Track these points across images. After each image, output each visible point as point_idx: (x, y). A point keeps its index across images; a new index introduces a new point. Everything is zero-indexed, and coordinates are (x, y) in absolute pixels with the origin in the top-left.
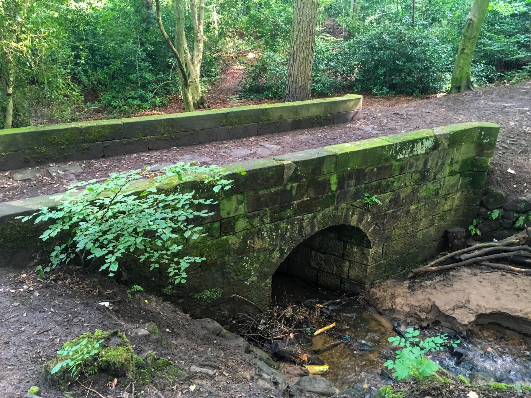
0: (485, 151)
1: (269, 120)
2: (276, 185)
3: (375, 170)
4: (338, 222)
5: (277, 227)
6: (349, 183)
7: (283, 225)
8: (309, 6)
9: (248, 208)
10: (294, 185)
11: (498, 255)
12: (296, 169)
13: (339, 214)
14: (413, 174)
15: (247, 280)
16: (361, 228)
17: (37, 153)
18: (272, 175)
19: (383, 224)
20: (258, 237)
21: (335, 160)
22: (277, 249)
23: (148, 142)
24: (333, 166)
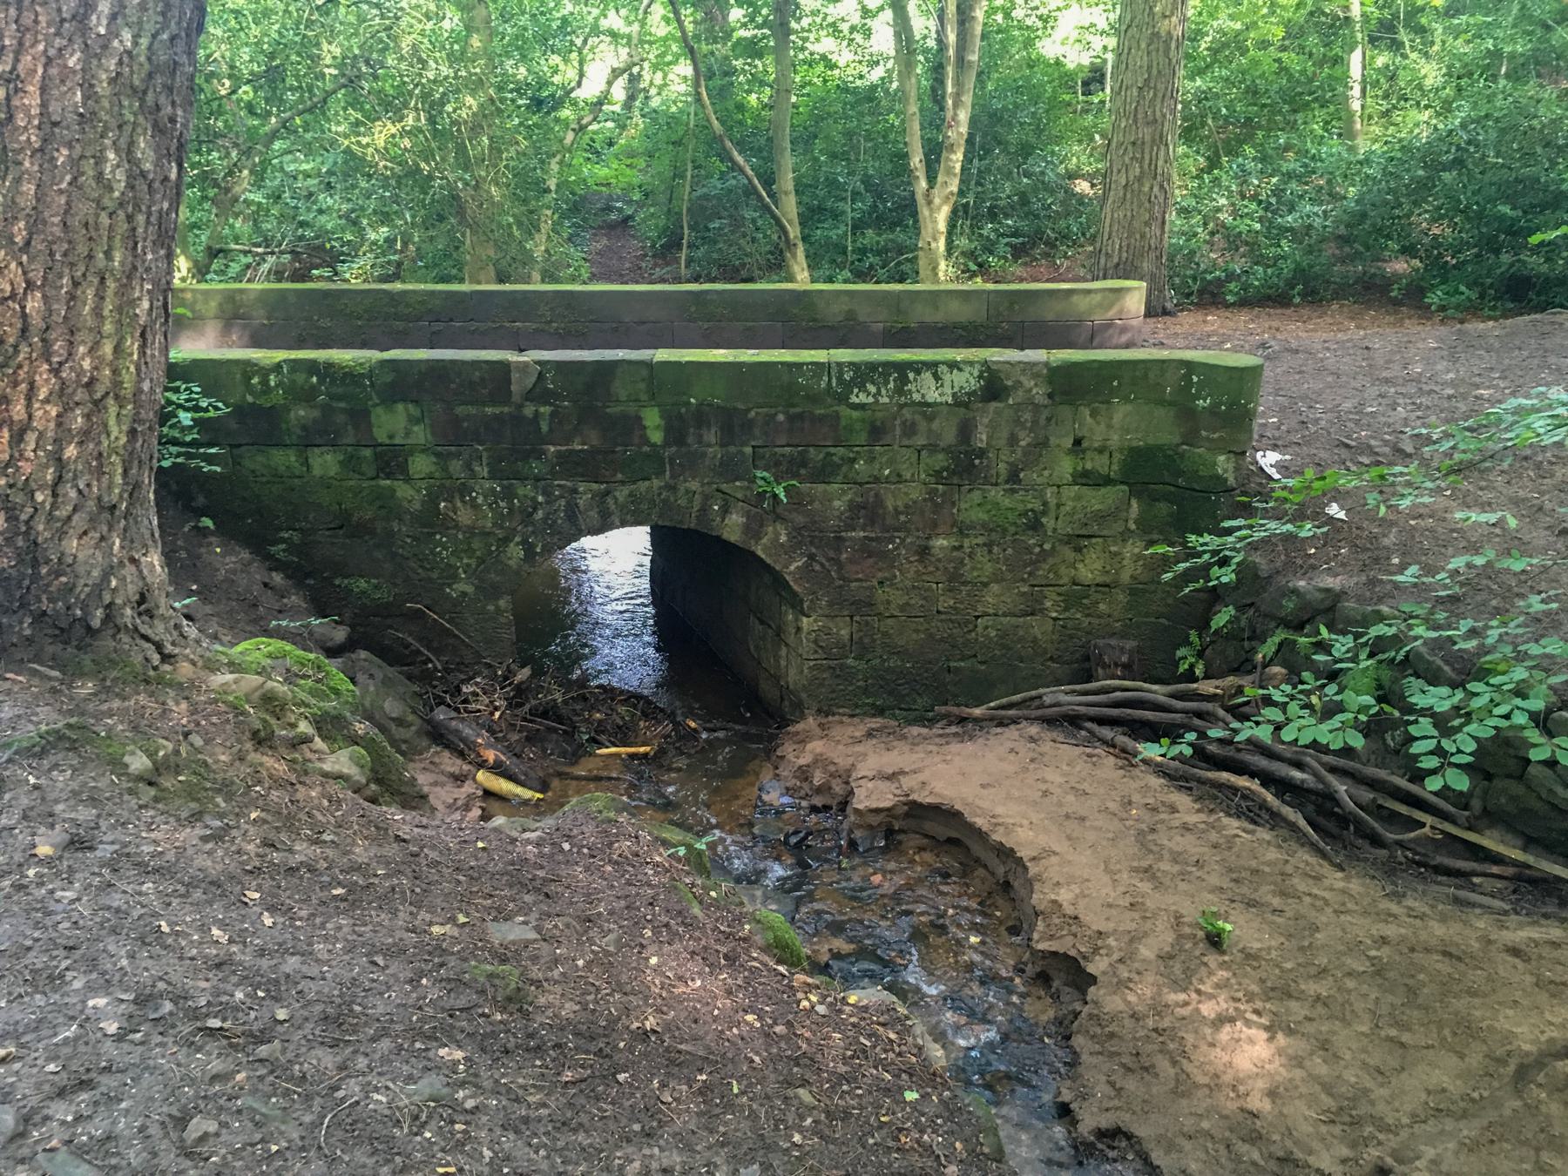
0: (1204, 433)
1: (814, 320)
2: (494, 403)
3: (781, 417)
4: (681, 522)
5: (508, 494)
6: (701, 436)
7: (525, 490)
8: (1143, 45)
9: (433, 434)
10: (542, 409)
11: (1129, 711)
12: (541, 375)
13: (682, 502)
14: (924, 453)
15: (449, 586)
16: (760, 553)
17: (318, 328)
18: (482, 379)
19: (836, 561)
20: (464, 502)
21: (645, 372)
22: (517, 539)
23: (517, 333)
24: (642, 386)
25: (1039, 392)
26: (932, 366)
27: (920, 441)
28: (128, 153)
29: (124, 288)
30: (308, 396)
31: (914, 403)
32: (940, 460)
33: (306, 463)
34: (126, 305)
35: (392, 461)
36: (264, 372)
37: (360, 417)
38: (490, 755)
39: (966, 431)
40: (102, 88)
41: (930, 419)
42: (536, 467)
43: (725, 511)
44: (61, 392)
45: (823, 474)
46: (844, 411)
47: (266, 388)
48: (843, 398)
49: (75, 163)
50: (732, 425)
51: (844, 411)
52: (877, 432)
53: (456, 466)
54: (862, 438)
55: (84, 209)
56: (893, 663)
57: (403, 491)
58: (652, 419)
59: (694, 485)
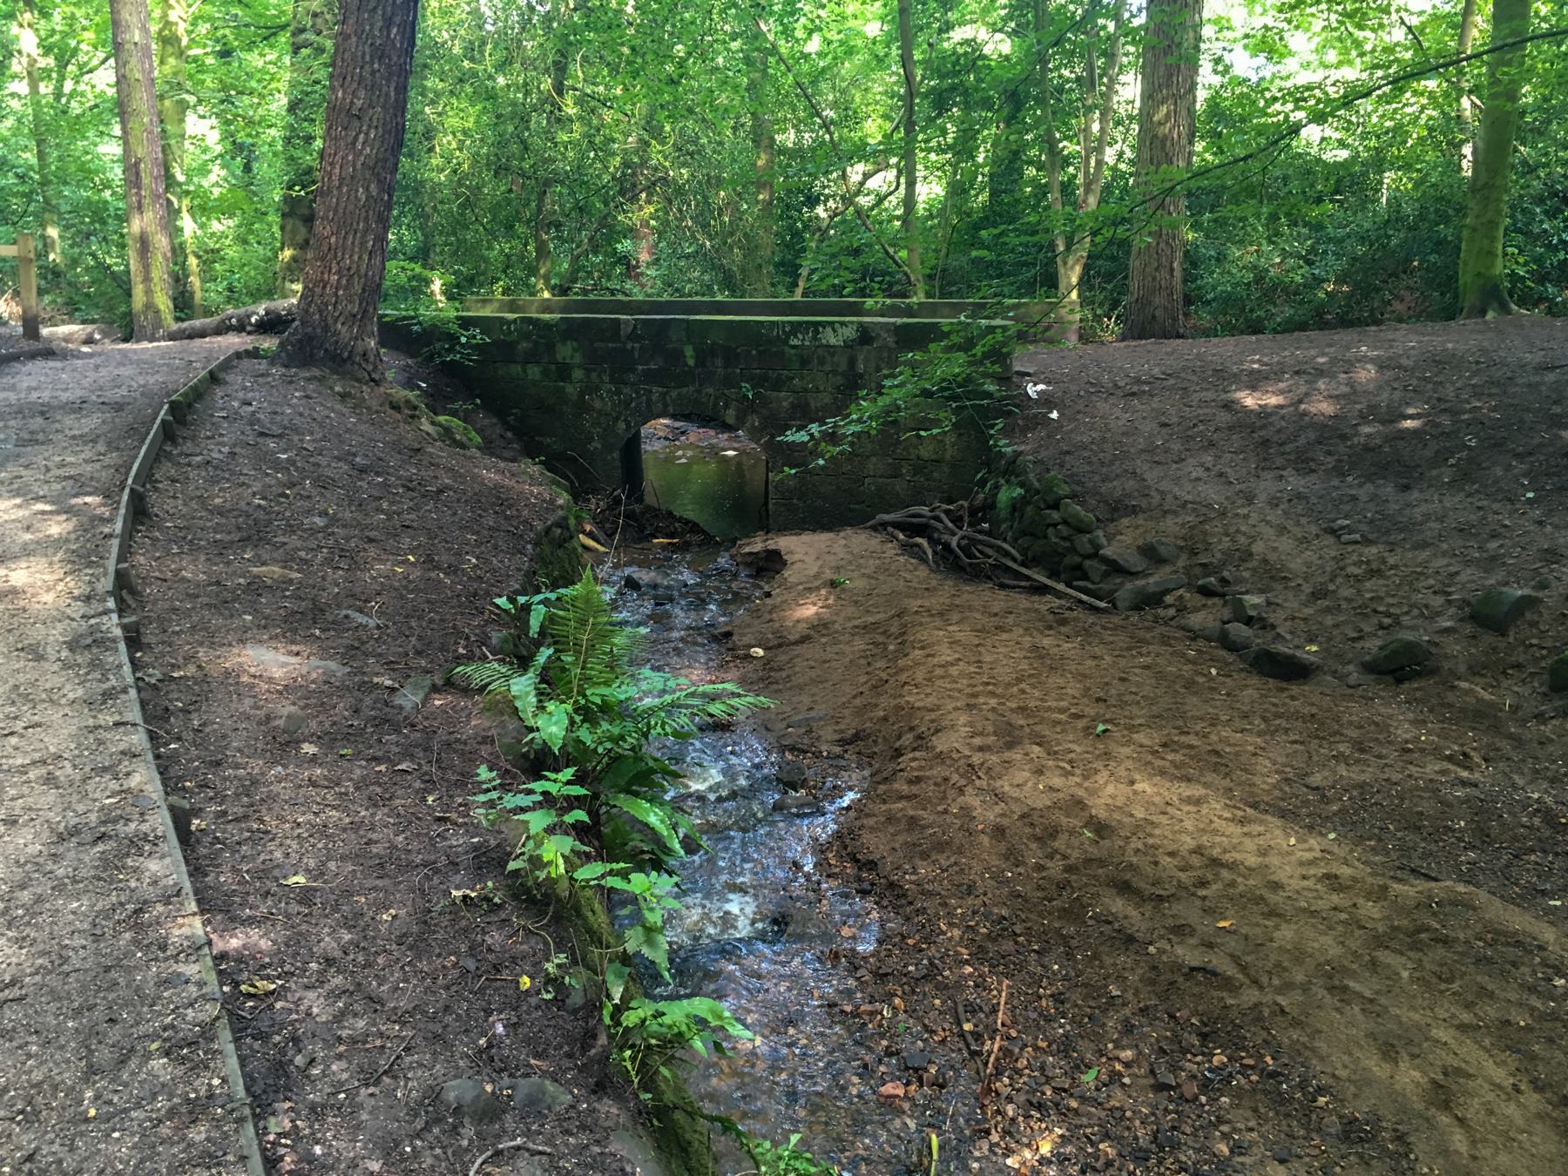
5: (618, 393)
25: (891, 340)
26: (832, 324)
27: (828, 368)
28: (367, 189)
29: (364, 236)
30: (526, 336)
31: (822, 346)
32: (840, 380)
33: (525, 371)
34: (363, 244)
35: (564, 372)
36: (509, 323)
37: (551, 348)
38: (588, 528)
39: (852, 362)
40: (359, 166)
41: (833, 355)
42: (632, 378)
43: (726, 406)
44: (339, 272)
45: (777, 386)
46: (787, 349)
47: (510, 333)
48: (786, 342)
49: (349, 192)
50: (730, 356)
51: (787, 349)
52: (804, 362)
53: (594, 375)
54: (797, 365)
55: (351, 207)
56: (819, 503)
57: (569, 389)
58: (689, 351)
59: (710, 390)
